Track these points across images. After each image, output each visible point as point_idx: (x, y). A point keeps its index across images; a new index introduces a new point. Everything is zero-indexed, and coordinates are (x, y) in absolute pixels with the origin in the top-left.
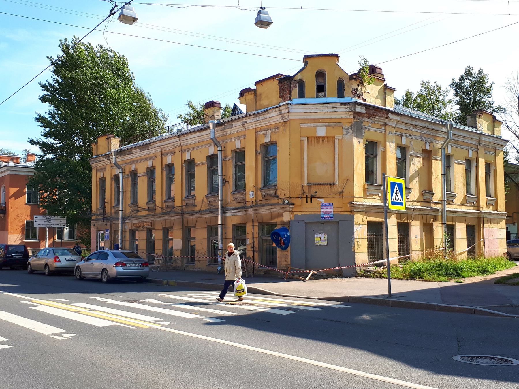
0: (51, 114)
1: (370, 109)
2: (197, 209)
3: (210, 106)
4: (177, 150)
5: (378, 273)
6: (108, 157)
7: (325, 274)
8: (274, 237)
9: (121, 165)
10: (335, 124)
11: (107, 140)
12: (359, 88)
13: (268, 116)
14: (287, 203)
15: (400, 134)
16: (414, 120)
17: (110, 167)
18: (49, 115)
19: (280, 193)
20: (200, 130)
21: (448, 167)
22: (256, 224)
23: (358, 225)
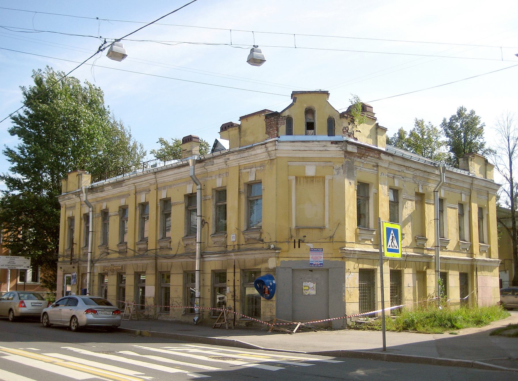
0: (20, 148)
1: (362, 149)
2: (173, 252)
3: (188, 140)
4: (153, 188)
5: (370, 325)
6: (78, 194)
7: (313, 326)
8: (258, 286)
9: (92, 203)
10: (326, 163)
11: (78, 176)
12: (350, 127)
13: (253, 153)
14: (273, 248)
15: (393, 175)
16: (406, 161)
17: (80, 205)
18: (18, 150)
19: (266, 237)
20: (179, 167)
21: (441, 212)
22: (238, 270)
23: (349, 273)
